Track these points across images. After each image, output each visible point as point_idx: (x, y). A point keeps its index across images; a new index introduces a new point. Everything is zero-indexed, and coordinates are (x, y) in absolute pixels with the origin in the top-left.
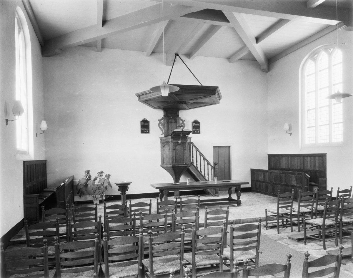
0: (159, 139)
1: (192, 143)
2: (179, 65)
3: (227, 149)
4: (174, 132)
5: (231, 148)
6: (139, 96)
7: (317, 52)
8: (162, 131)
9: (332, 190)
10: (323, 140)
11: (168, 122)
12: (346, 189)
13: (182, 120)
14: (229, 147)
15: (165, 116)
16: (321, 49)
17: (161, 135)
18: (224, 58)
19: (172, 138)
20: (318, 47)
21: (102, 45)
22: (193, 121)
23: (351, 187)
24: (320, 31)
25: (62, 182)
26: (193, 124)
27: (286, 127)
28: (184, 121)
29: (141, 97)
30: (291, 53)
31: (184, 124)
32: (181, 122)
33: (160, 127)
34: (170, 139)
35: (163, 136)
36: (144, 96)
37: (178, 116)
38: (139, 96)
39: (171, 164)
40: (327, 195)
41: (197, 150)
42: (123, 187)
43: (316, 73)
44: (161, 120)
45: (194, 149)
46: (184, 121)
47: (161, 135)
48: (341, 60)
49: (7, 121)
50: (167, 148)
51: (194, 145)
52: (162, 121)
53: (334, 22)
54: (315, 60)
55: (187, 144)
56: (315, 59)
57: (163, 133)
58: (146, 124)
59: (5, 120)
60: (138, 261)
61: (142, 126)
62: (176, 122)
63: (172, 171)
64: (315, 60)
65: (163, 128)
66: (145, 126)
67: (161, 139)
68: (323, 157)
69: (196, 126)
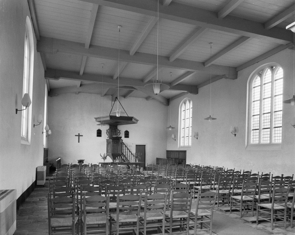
0: (106, 140)
1: (123, 143)
2: (117, 103)
3: (144, 146)
4: (113, 137)
5: (146, 146)
6: (96, 119)
7: (263, 70)
8: (108, 136)
9: (293, 176)
10: (186, 144)
11: (111, 131)
12: (279, 176)
13: (119, 130)
14: (145, 145)
15: (110, 128)
16: (266, 67)
17: (108, 138)
18: (172, 82)
19: (112, 140)
20: (265, 64)
21: (99, 46)
22: (125, 131)
23: (293, 175)
24: (274, 49)
25: (135, 195)
26: (125, 133)
27: (173, 136)
28: (120, 131)
29: (97, 119)
30: (123, 125)
31: (120, 133)
32: (119, 131)
33: (107, 134)
34: (111, 140)
35: (108, 138)
36: (99, 119)
37: (117, 128)
38: (96, 119)
39: (111, 153)
40: (242, 177)
41: (126, 146)
42: (81, 161)
43: (261, 86)
44: (108, 130)
45: (124, 146)
46: (120, 131)
47: (108, 138)
48: (282, 76)
49: (17, 110)
50: (109, 145)
51: (124, 144)
52: (108, 131)
53: (186, 91)
54: (260, 75)
55: (120, 143)
56: (260, 74)
57: (108, 137)
58: (100, 132)
59: (15, 110)
60: (79, 185)
61: (98, 133)
62: (115, 132)
63: (112, 157)
64: (260, 75)
65: (109, 134)
66: (99, 133)
67: (107, 140)
68: (185, 152)
69: (127, 134)
